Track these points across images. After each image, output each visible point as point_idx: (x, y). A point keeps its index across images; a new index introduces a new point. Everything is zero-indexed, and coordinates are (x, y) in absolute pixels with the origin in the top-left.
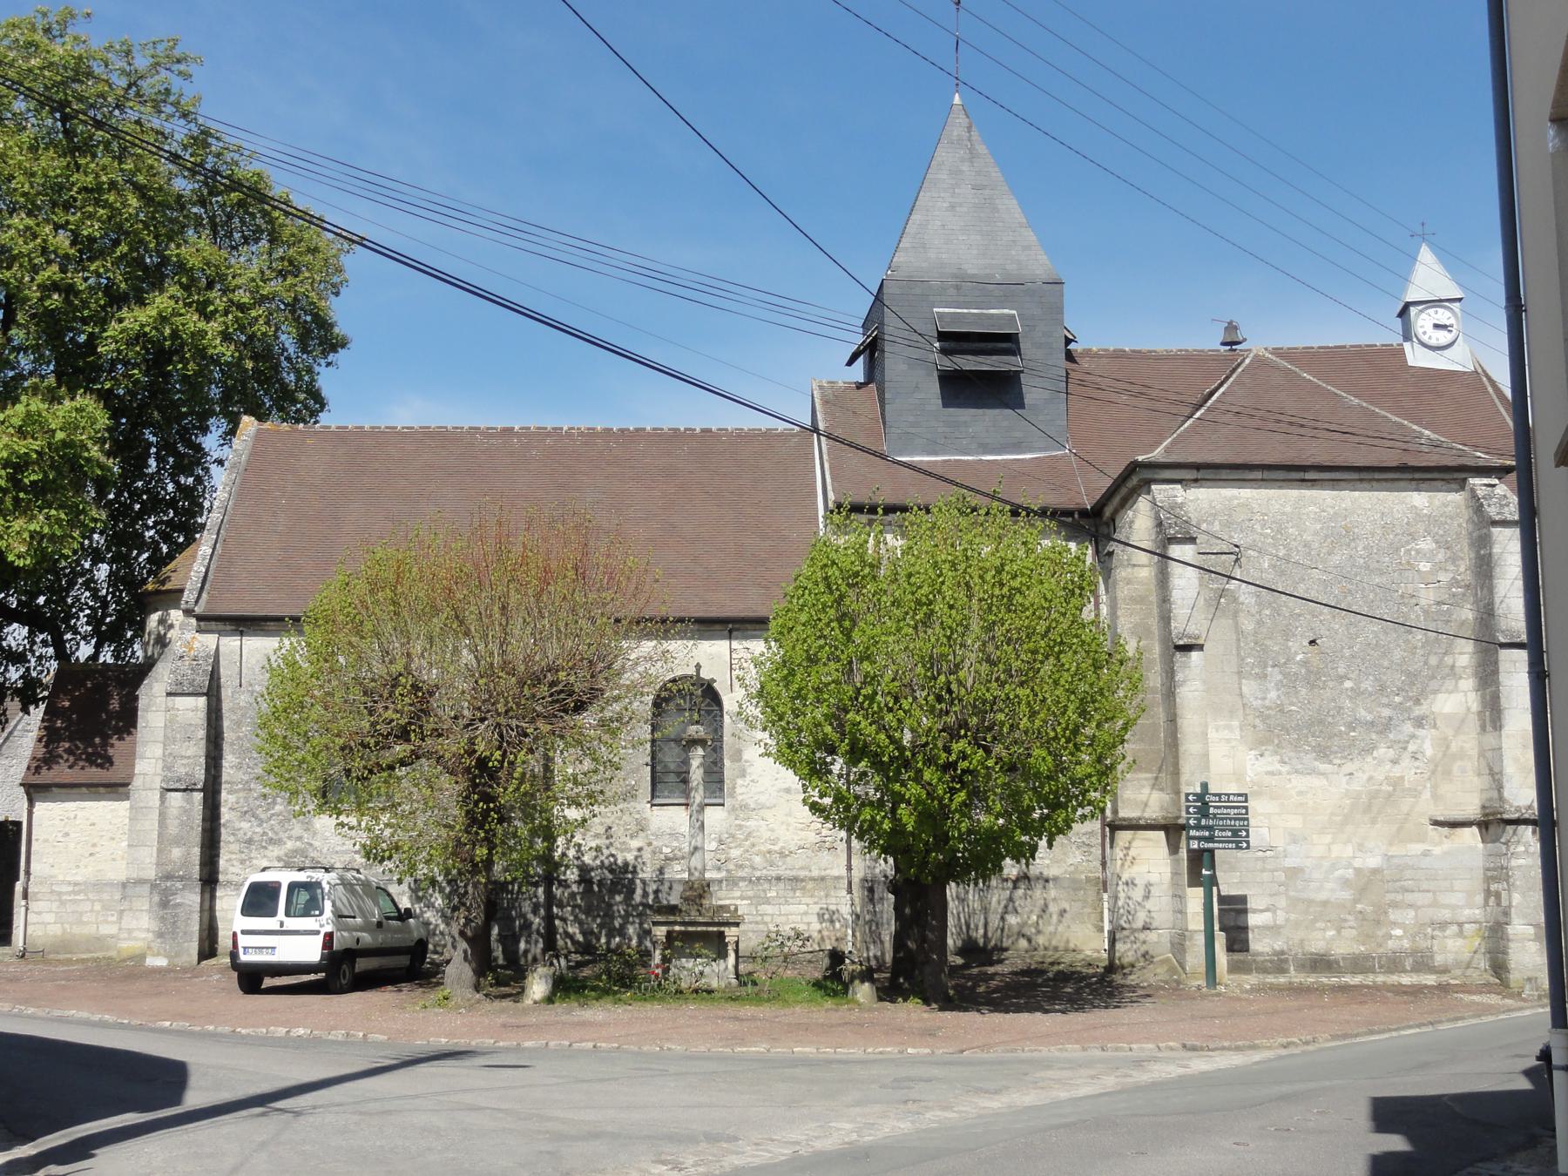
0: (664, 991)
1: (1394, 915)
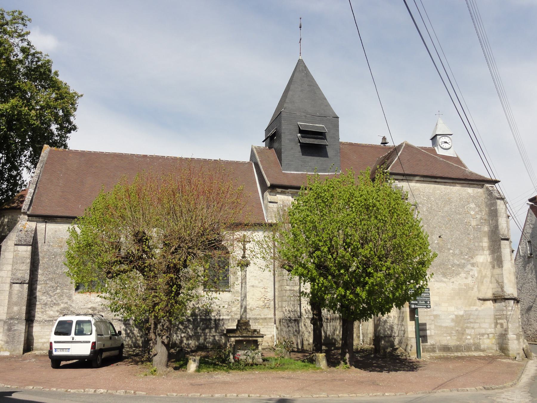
0: (239, 365)
1: (468, 331)
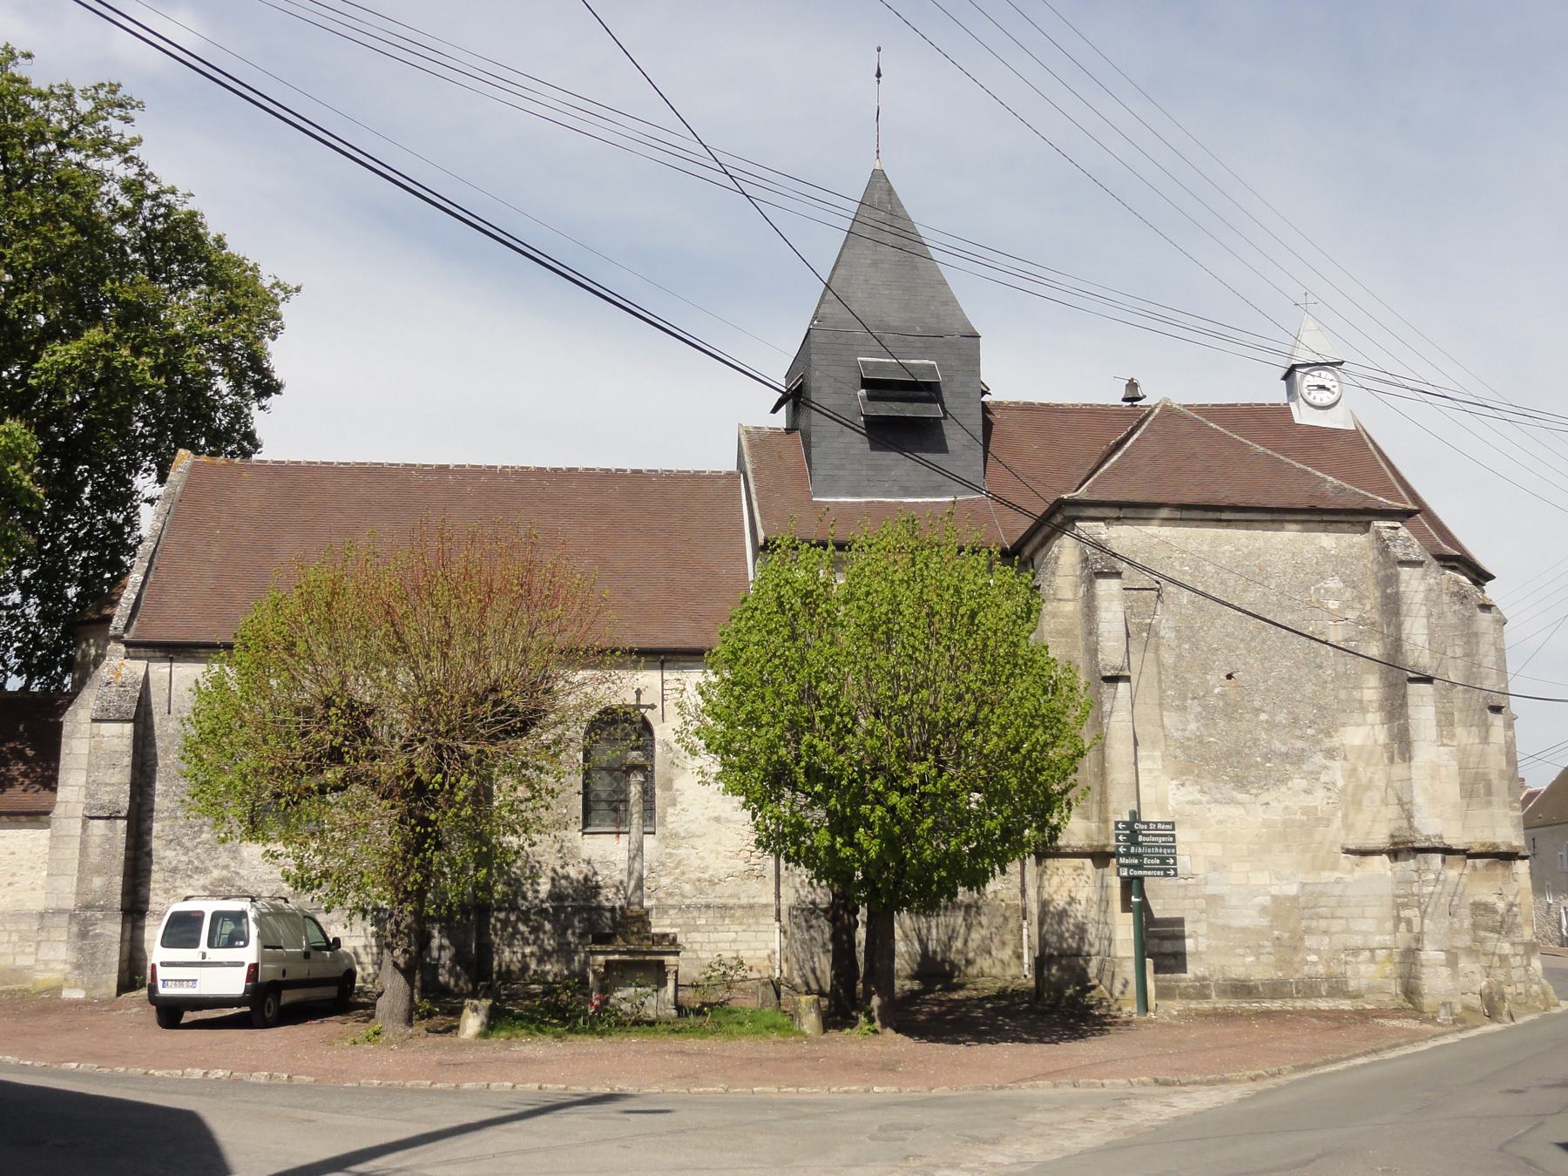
1: (1310, 941)
